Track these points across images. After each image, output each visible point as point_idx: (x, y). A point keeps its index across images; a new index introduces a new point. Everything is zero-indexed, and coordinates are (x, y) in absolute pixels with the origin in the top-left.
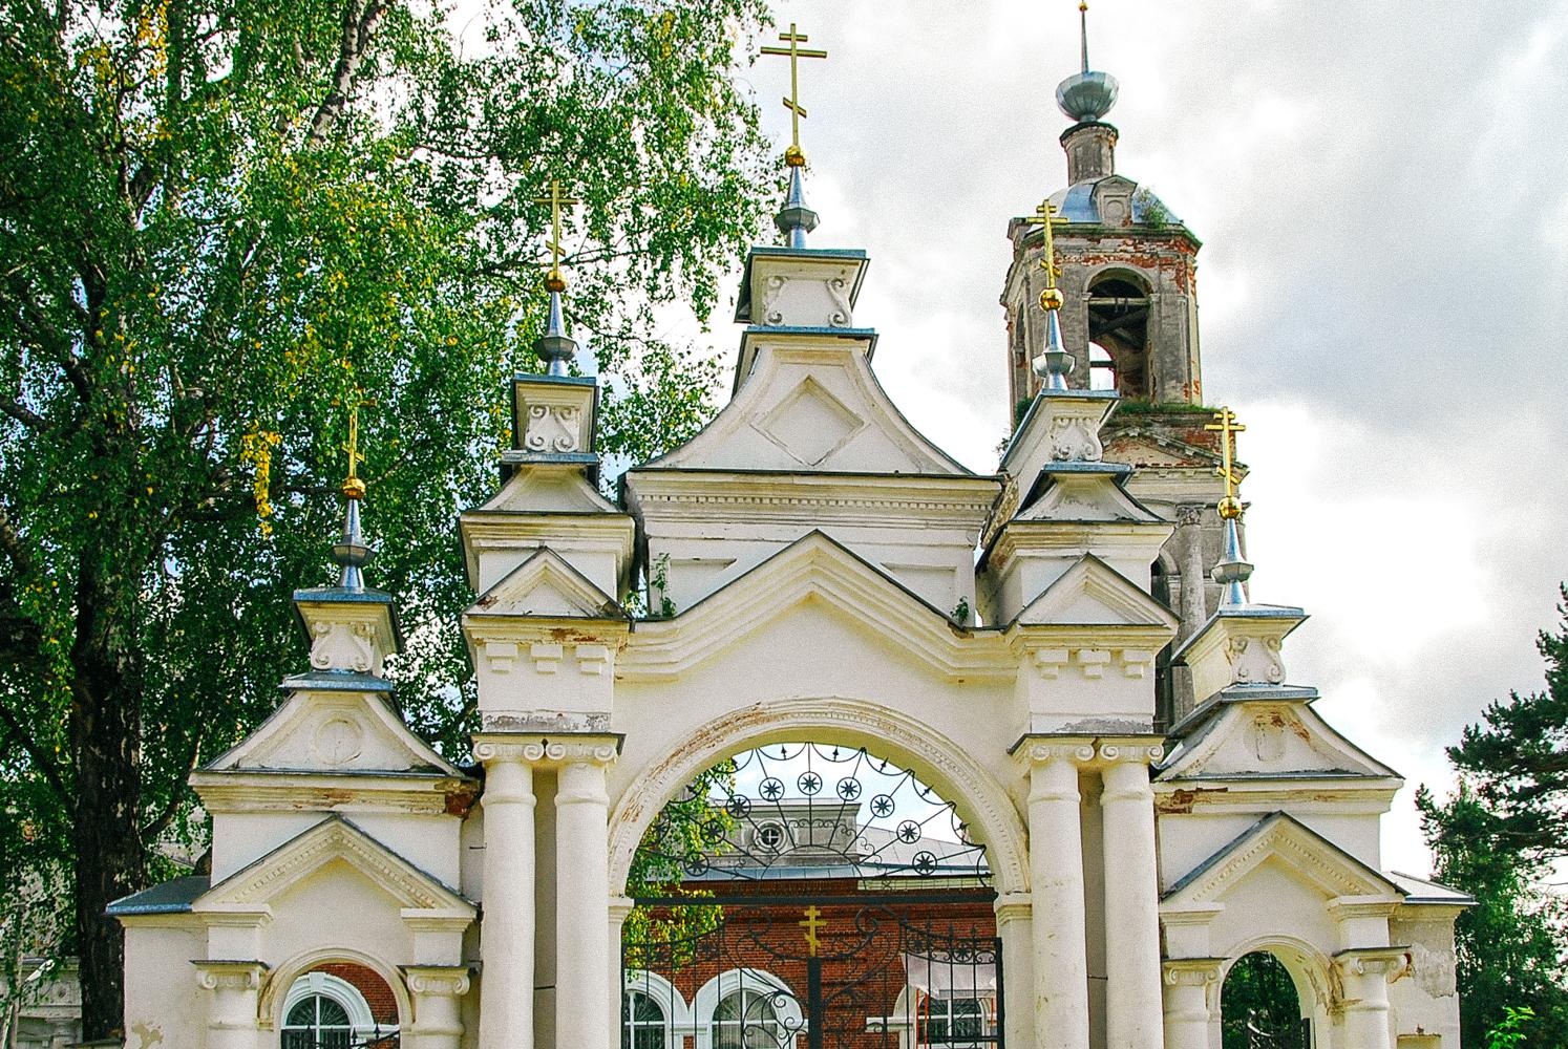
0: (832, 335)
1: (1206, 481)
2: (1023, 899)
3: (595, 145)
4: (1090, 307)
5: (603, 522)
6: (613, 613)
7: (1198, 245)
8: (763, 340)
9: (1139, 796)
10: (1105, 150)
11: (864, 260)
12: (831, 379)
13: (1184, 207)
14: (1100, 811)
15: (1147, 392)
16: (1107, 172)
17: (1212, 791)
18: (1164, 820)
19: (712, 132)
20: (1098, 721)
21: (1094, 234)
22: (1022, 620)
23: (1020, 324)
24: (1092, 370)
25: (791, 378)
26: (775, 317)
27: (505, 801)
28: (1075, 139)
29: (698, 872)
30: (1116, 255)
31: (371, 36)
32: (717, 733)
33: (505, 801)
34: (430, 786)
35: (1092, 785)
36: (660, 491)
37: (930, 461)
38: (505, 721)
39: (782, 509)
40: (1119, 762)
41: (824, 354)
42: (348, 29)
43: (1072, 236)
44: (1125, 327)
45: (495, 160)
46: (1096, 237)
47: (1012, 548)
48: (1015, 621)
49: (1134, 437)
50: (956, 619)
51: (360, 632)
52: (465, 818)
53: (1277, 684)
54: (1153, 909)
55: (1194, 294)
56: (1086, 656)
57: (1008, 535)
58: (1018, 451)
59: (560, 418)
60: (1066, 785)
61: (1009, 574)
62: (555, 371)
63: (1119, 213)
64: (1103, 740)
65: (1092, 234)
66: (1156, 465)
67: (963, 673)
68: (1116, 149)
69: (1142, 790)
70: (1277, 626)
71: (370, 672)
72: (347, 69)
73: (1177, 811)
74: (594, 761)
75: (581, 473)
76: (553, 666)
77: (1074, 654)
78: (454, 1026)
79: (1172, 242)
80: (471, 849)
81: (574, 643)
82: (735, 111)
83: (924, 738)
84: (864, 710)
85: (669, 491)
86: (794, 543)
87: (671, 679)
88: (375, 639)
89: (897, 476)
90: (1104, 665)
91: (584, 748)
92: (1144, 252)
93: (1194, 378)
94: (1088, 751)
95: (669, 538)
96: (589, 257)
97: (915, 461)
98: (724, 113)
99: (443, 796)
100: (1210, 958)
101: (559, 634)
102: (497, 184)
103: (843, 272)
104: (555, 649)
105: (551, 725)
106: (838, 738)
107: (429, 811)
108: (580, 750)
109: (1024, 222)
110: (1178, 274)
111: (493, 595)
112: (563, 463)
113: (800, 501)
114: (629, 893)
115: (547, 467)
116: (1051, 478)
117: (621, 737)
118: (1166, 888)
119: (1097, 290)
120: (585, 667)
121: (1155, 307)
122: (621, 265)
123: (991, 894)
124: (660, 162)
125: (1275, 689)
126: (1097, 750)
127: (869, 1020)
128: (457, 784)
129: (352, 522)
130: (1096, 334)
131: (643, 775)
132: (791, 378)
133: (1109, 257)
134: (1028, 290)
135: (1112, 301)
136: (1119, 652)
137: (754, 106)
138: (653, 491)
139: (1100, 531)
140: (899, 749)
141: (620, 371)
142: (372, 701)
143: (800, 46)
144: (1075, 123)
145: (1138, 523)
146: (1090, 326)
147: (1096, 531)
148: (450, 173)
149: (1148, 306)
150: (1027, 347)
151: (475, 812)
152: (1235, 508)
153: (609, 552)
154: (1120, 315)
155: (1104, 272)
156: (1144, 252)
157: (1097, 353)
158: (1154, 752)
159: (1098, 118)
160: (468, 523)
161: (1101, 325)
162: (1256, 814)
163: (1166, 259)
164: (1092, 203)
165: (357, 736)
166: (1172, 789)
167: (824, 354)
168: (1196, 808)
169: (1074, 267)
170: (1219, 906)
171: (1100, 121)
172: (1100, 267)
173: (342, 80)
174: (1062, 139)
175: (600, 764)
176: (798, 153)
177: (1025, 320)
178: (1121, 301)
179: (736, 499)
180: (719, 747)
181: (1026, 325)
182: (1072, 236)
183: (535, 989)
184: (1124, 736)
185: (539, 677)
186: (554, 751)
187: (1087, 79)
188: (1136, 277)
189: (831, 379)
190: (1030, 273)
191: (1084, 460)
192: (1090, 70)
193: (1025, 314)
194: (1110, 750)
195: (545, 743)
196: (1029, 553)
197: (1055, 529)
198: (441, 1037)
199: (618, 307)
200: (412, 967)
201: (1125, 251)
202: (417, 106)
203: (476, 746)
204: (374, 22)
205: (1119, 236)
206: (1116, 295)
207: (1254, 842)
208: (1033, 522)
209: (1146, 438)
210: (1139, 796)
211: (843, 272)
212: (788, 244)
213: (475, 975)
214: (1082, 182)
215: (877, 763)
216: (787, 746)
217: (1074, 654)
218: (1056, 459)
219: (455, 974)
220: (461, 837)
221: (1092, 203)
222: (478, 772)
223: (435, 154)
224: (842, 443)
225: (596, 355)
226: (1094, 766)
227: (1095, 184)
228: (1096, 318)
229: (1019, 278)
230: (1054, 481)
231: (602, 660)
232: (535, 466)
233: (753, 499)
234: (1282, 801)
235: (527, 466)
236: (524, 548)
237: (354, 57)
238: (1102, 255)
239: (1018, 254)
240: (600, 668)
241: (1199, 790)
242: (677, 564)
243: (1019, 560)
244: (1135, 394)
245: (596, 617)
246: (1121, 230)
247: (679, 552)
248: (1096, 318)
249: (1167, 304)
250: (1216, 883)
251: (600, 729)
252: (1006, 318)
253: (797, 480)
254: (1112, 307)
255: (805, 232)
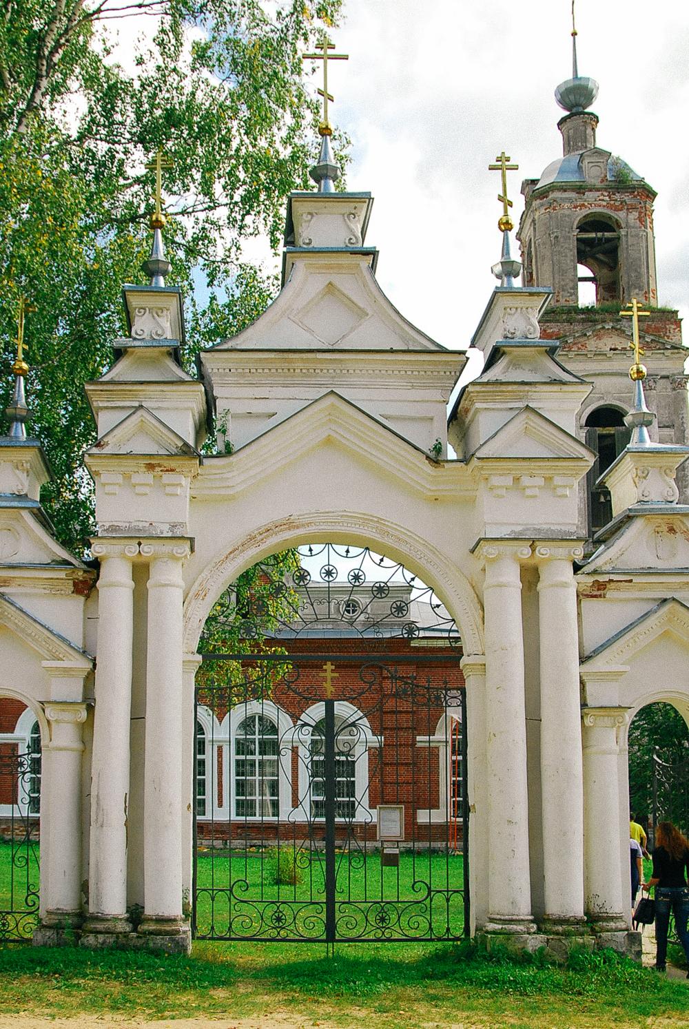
0: (346, 252)
1: (660, 359)
2: (479, 660)
3: (205, 131)
4: (578, 239)
5: (182, 388)
6: (186, 451)
7: (654, 195)
8: (296, 257)
9: (565, 585)
10: (589, 131)
11: (370, 199)
12: (346, 284)
13: (642, 168)
14: (537, 596)
15: (619, 298)
16: (590, 146)
17: (621, 581)
18: (586, 603)
19: (288, 120)
20: (535, 529)
21: (580, 189)
22: (478, 455)
23: (530, 253)
24: (580, 284)
25: (316, 284)
26: (307, 241)
27: (111, 585)
28: (569, 124)
29: (400, 615)
30: (596, 203)
31: (55, 64)
32: (261, 537)
33: (111, 585)
34: (62, 575)
35: (531, 577)
36: (224, 365)
37: (415, 340)
38: (113, 528)
39: (310, 377)
40: (550, 560)
41: (340, 267)
42: (40, 61)
43: (565, 191)
44: (604, 253)
45: (140, 146)
46: (582, 191)
47: (473, 403)
48: (473, 455)
49: (608, 329)
50: (432, 455)
51: (20, 468)
52: (88, 597)
53: (671, 502)
54: (575, 668)
55: (652, 229)
56: (526, 481)
57: (469, 393)
58: (482, 333)
59: (156, 315)
60: (512, 577)
61: (472, 421)
62: (156, 283)
63: (598, 174)
64: (537, 543)
65: (579, 189)
66: (624, 349)
67: (437, 494)
68: (597, 130)
69: (567, 580)
70: (671, 459)
71: (26, 495)
72: (39, 88)
73: (595, 596)
74: (174, 558)
75: (169, 354)
76: (147, 490)
77: (517, 480)
78: (77, 745)
79: (636, 193)
80: (90, 618)
81: (161, 473)
82: (305, 106)
83: (409, 540)
84: (366, 520)
85: (230, 365)
86: (316, 401)
87: (231, 498)
88: (31, 472)
89: (392, 351)
90: (540, 488)
91: (168, 547)
92: (616, 200)
93: (651, 287)
94: (527, 552)
95: (229, 399)
96: (200, 207)
97: (404, 339)
98: (298, 107)
99: (71, 582)
100: (620, 707)
101: (151, 467)
102: (137, 162)
103: (355, 208)
104: (149, 477)
105: (145, 531)
106: (349, 540)
107: (63, 592)
108: (164, 549)
109: (534, 182)
110: (640, 215)
111: (105, 440)
112: (155, 346)
113: (322, 370)
114: (199, 652)
115: (145, 350)
116: (501, 352)
117: (192, 540)
118: (587, 653)
119: (583, 228)
120: (169, 490)
121: (624, 239)
122: (221, 214)
123: (459, 652)
124: (247, 141)
125: (669, 506)
126: (533, 551)
127: (419, 738)
128: (81, 573)
129: (19, 391)
130: (582, 258)
131: (210, 567)
132: (316, 284)
133: (591, 204)
134: (535, 228)
135: (593, 235)
136: (551, 478)
137: (318, 101)
138: (219, 366)
139: (537, 389)
140: (392, 548)
141: (223, 285)
142: (27, 516)
143: (330, 52)
144: (568, 113)
145: (564, 383)
146: (578, 252)
147: (534, 389)
148: (111, 154)
149: (619, 238)
150: (534, 268)
151: (93, 594)
152: (642, 372)
153: (187, 409)
154: (599, 244)
155: (588, 215)
156: (616, 200)
157: (583, 271)
158: (577, 552)
159: (584, 109)
160: (90, 390)
161: (585, 253)
162: (655, 600)
163: (631, 205)
164: (580, 168)
165: (17, 540)
166: (590, 580)
167: (340, 267)
168: (609, 594)
169: (567, 212)
170: (627, 668)
171: (586, 111)
172: (585, 212)
173: (36, 95)
174: (559, 124)
175: (177, 559)
176: (327, 126)
177: (533, 249)
178: (599, 235)
179: (277, 370)
180: (263, 547)
181: (533, 253)
182: (565, 191)
183: (131, 719)
184: (553, 540)
185: (107, 496)
186: (146, 550)
187: (577, 82)
188: (610, 218)
189: (346, 284)
190: (536, 217)
191: (527, 338)
192: (579, 76)
193: (533, 245)
194: (543, 550)
195: (140, 544)
196: (485, 406)
197: (503, 388)
198: (70, 752)
199: (219, 242)
200: (49, 702)
201: (603, 200)
202: (91, 111)
203: (93, 546)
204: (57, 55)
205: (598, 190)
206: (596, 231)
207: (652, 621)
208: (488, 383)
209: (617, 330)
210: (565, 585)
211: (355, 208)
212: (319, 190)
213: (91, 709)
214: (572, 154)
215: (377, 558)
216: (313, 547)
217: (517, 480)
218: (506, 337)
219: (77, 707)
220: (84, 611)
221: (580, 168)
222: (95, 565)
223: (98, 142)
224: (353, 329)
225: (208, 275)
226: (532, 562)
227: (582, 155)
228: (582, 247)
229: (529, 221)
230: (504, 353)
231: (180, 485)
232: (136, 349)
233: (289, 370)
234: (675, 590)
235: (133, 349)
236: (129, 407)
237: (44, 79)
238: (586, 204)
239: (528, 204)
240: (179, 491)
241: (611, 581)
242: (235, 416)
243: (477, 410)
244: (610, 299)
245: (176, 455)
246: (599, 185)
247: (238, 408)
248: (582, 247)
249: (632, 236)
250: (624, 650)
251: (178, 534)
252: (520, 249)
253: (320, 356)
254: (593, 239)
255: (331, 181)
